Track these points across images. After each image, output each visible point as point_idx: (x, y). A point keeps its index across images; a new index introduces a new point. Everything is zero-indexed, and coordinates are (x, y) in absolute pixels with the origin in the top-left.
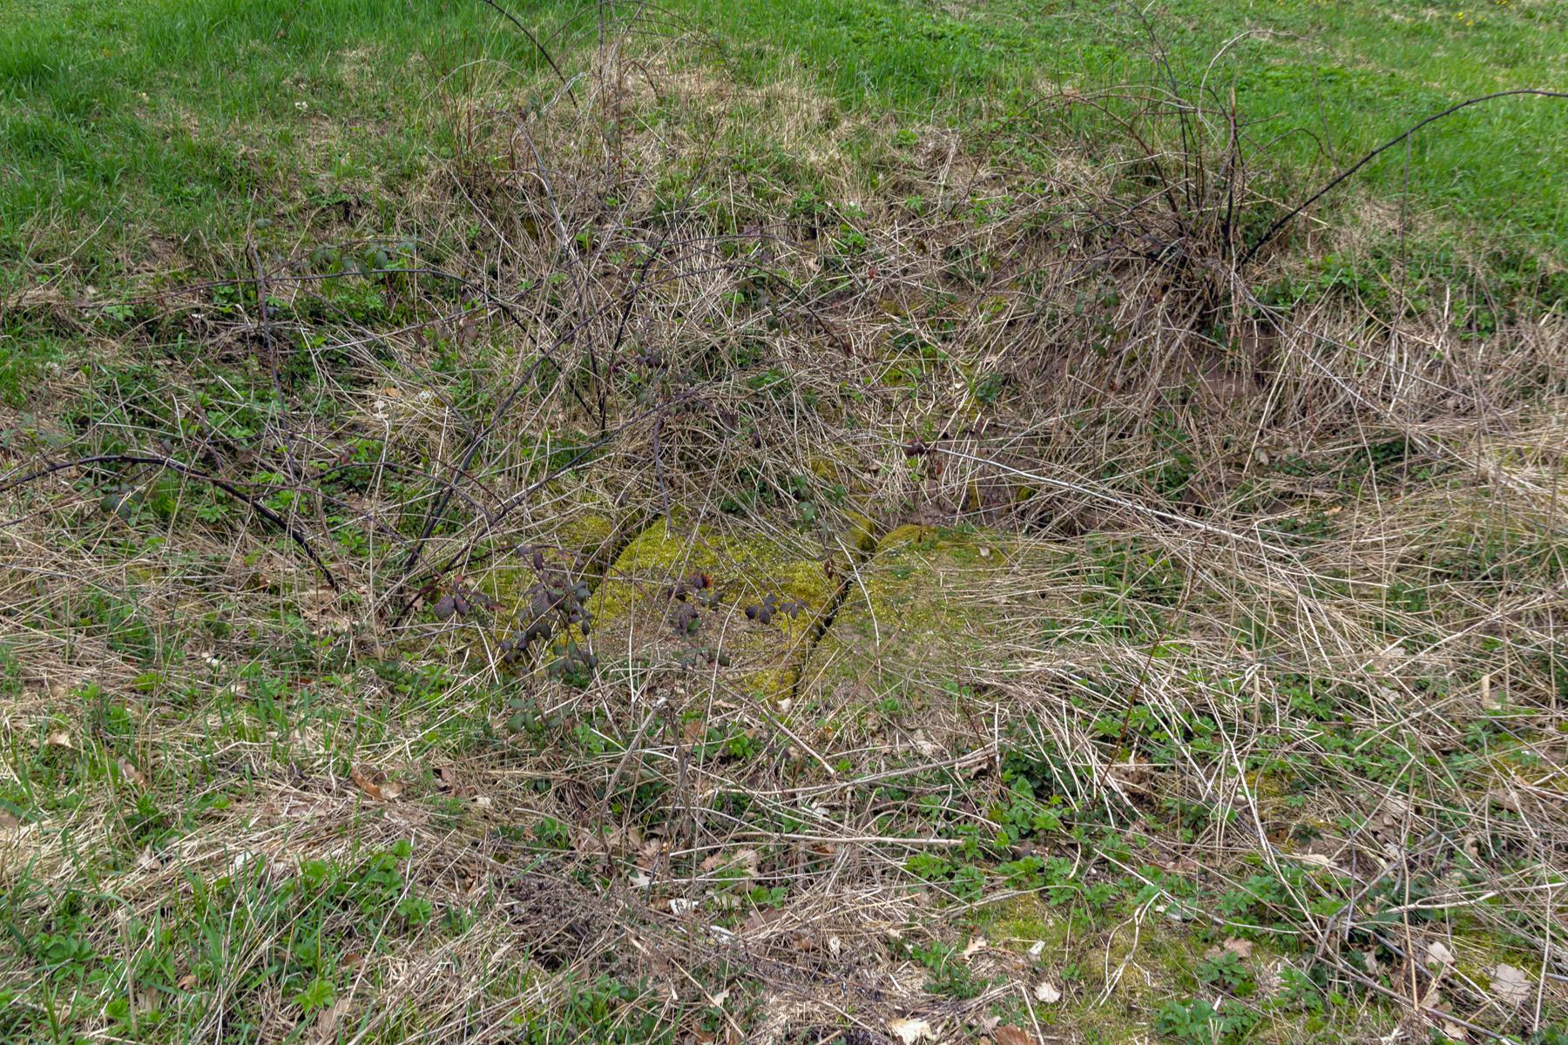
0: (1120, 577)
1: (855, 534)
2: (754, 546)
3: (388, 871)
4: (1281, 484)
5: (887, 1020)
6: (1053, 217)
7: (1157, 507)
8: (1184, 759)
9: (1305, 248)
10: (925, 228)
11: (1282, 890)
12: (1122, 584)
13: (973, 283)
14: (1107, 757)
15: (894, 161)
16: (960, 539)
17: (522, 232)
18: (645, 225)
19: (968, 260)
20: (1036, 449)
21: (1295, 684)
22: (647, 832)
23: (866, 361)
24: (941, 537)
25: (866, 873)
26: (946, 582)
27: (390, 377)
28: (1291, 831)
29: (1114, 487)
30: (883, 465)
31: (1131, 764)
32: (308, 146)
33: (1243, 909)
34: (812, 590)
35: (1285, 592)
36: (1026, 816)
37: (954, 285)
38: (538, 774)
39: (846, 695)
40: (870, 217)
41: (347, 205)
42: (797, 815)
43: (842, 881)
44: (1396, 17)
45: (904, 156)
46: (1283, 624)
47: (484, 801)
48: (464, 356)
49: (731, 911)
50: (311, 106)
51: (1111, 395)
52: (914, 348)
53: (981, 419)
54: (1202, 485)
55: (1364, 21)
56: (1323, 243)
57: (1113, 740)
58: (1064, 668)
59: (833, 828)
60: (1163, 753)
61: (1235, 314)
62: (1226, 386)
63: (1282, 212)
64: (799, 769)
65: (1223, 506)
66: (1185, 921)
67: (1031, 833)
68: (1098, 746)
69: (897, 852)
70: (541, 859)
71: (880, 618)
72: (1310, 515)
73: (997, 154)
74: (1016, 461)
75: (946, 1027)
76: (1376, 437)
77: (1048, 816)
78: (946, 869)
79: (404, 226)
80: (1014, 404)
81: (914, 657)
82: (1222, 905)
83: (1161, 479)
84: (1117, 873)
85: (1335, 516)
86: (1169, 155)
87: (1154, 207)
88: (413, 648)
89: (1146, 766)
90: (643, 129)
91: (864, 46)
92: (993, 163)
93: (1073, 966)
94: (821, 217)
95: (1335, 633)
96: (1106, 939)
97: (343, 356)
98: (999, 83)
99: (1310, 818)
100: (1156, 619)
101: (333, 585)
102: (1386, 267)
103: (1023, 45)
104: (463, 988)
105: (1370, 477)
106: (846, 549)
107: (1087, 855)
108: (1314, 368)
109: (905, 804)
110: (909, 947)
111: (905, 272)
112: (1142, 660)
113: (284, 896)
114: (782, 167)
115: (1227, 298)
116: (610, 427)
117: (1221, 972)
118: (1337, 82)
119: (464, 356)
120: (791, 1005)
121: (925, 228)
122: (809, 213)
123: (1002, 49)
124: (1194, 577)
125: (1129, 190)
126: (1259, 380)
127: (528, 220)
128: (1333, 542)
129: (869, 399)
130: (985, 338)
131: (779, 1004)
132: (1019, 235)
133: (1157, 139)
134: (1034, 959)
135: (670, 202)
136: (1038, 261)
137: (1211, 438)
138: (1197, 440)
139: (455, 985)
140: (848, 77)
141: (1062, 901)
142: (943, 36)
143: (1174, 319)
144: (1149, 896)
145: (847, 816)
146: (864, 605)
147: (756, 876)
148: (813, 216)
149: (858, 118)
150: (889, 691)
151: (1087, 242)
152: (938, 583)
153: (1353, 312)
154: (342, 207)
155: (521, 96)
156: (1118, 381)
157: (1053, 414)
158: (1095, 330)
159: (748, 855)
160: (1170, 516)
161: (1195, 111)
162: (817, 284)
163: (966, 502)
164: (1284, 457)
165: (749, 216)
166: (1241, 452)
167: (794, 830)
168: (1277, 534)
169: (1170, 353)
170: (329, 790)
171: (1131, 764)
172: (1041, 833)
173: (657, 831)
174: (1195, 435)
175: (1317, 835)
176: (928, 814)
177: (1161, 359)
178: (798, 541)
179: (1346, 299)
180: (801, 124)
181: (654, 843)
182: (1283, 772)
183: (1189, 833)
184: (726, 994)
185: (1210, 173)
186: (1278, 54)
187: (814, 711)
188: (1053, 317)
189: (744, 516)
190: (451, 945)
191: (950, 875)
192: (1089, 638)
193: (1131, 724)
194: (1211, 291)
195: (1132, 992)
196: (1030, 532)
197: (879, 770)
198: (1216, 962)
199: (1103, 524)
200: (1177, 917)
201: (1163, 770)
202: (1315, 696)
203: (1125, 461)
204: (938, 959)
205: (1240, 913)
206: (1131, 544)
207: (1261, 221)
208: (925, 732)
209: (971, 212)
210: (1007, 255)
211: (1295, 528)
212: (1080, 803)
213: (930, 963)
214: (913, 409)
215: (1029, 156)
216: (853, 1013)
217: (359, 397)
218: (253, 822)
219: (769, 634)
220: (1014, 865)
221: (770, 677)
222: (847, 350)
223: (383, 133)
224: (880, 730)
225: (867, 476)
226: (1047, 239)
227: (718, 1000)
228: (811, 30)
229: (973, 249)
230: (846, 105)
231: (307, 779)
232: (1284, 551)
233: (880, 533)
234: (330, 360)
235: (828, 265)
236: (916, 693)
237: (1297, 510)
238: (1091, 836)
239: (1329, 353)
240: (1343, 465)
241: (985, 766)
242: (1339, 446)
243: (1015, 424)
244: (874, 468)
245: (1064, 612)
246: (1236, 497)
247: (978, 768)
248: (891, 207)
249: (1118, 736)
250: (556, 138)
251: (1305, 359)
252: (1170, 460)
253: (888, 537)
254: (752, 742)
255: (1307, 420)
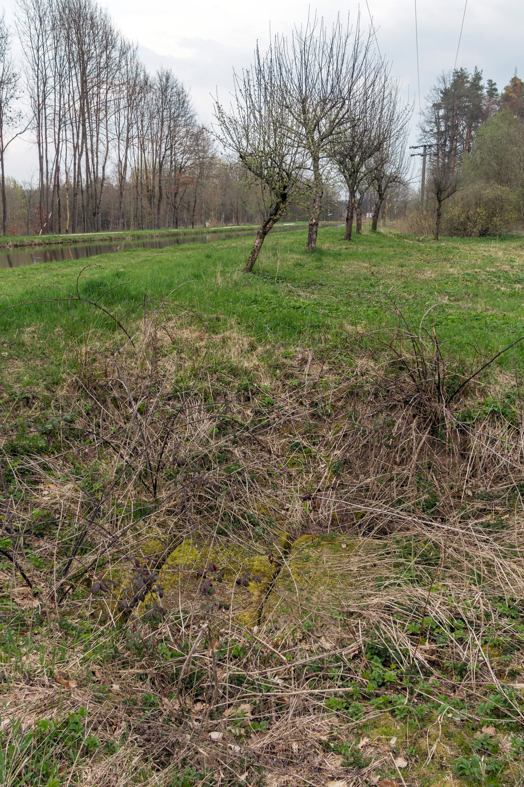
0: (410, 554)
1: (281, 541)
2: (233, 550)
3: (77, 723)
4: (479, 505)
5: (326, 782)
6: (359, 387)
7: (424, 519)
8: (452, 641)
9: (475, 395)
10: (301, 393)
11: (505, 701)
12: (411, 558)
13: (325, 418)
14: (415, 643)
15: (284, 364)
16: (331, 540)
17: (111, 406)
18: (169, 399)
19: (322, 408)
20: (362, 494)
21: (499, 601)
22: (195, 699)
23: (278, 456)
24: (322, 540)
25: (305, 711)
26: (327, 562)
27: (51, 479)
28: (507, 673)
29: (401, 510)
30: (291, 506)
31: (427, 646)
32: (8, 372)
33: (489, 711)
34: (263, 570)
35: (488, 556)
36: (380, 675)
37: (316, 419)
38: (141, 671)
39: (285, 622)
40: (274, 390)
41: (28, 398)
42: (269, 683)
43: (294, 715)
44: (503, 289)
45: (288, 362)
46: (489, 572)
47: (116, 687)
48: (85, 466)
49: (241, 736)
50: (10, 354)
51: (395, 467)
52: (300, 449)
53: (335, 481)
54: (443, 507)
55: (488, 291)
56: (483, 392)
57: (417, 635)
58: (389, 600)
59: (288, 688)
60: (441, 639)
61: (447, 426)
62: (448, 460)
63: (463, 380)
64: (266, 661)
65: (454, 517)
66: (462, 720)
67: (383, 684)
68: (410, 638)
69: (319, 698)
70: (148, 713)
71: (297, 582)
72: (495, 519)
73: (330, 359)
74: (354, 500)
75: (355, 783)
76: (520, 480)
77: (391, 674)
78: (345, 705)
79: (55, 407)
80: (350, 473)
81: (316, 600)
82: (479, 711)
83: (423, 505)
84: (427, 700)
85: (507, 519)
86: (407, 356)
87: (405, 380)
88: (69, 614)
89: (434, 646)
90: (166, 355)
91: (265, 313)
92: (329, 363)
93: (412, 748)
94: (252, 391)
95: (514, 575)
96: (426, 732)
97: (27, 470)
98: (328, 328)
99: (515, 666)
100: (429, 574)
101: (29, 584)
102: (513, 402)
103: (336, 309)
104: (119, 780)
105: (520, 500)
106: (278, 548)
107: (411, 693)
108: (487, 450)
109: (321, 674)
110: (332, 745)
111: (293, 414)
112: (426, 594)
113: (29, 739)
114: (232, 370)
115: (443, 419)
116: (158, 496)
117: (482, 744)
118: (480, 320)
119: (85, 466)
120: (278, 778)
121: (301, 393)
122: (246, 389)
123: (327, 311)
124: (445, 552)
125: (392, 372)
126: (463, 456)
127: (114, 400)
128: (507, 531)
129: (281, 474)
130: (333, 443)
131: (272, 778)
132: (344, 395)
133: (402, 349)
134: (392, 746)
135: (181, 388)
136: (355, 405)
137: (444, 485)
138: (438, 486)
139: (115, 779)
140: (259, 327)
141: (402, 716)
142: (300, 307)
143: (420, 430)
144: (444, 709)
145: (293, 682)
146: (289, 576)
147: (252, 717)
148: (248, 391)
149: (265, 345)
150: (306, 618)
151: (376, 395)
152: (323, 563)
153: (501, 423)
154: (25, 400)
155: (108, 344)
156: (398, 460)
157: (369, 477)
158: (385, 437)
159: (246, 707)
160: (430, 523)
161: (418, 338)
162: (252, 422)
163: (332, 522)
164: (479, 492)
165: (218, 392)
166: (459, 491)
167: (268, 691)
168: (481, 529)
169: (420, 446)
170: (44, 685)
171: (427, 646)
172: (388, 684)
173: (200, 698)
174: (436, 483)
175: (519, 674)
176: (333, 678)
177: (416, 448)
178: (254, 546)
179: (497, 417)
180: (240, 350)
181: (199, 704)
182: (499, 645)
183: (459, 678)
184: (246, 774)
185: (428, 364)
186: (451, 307)
187: (270, 631)
188: (364, 431)
189: (226, 535)
190: (111, 759)
191: (347, 708)
192: (399, 585)
193: (425, 626)
194: (435, 417)
195: (441, 758)
196: (364, 535)
197: (306, 658)
198: (479, 739)
199: (399, 529)
200: (458, 719)
201: (443, 648)
202: (509, 607)
203: (405, 497)
204: (346, 750)
205: (487, 714)
206: (413, 538)
207: (454, 384)
208: (325, 638)
209: (321, 385)
210: (340, 404)
211: (489, 526)
212: (405, 667)
213: (343, 752)
214: (302, 478)
215: (345, 359)
216: (308, 780)
217: (35, 490)
218: (8, 704)
219: (244, 594)
220: (377, 700)
221: (247, 615)
222: (269, 452)
223: (44, 364)
224: (303, 638)
225: (283, 512)
226: (357, 396)
227: (243, 778)
228: (240, 308)
229: (324, 402)
230: (259, 340)
231: (33, 681)
232: (486, 537)
233: (292, 540)
234: (21, 473)
235: (257, 413)
236: (319, 618)
237: (489, 517)
238: (412, 683)
239: (493, 442)
240: (507, 495)
241: (357, 652)
242: (504, 485)
243: (352, 483)
244: (286, 508)
245: (386, 573)
246: (459, 512)
247: (353, 654)
248: (284, 385)
249: (419, 632)
250: (126, 362)
251: (482, 446)
252: (426, 496)
253: (296, 542)
254: (242, 648)
255: (487, 474)
